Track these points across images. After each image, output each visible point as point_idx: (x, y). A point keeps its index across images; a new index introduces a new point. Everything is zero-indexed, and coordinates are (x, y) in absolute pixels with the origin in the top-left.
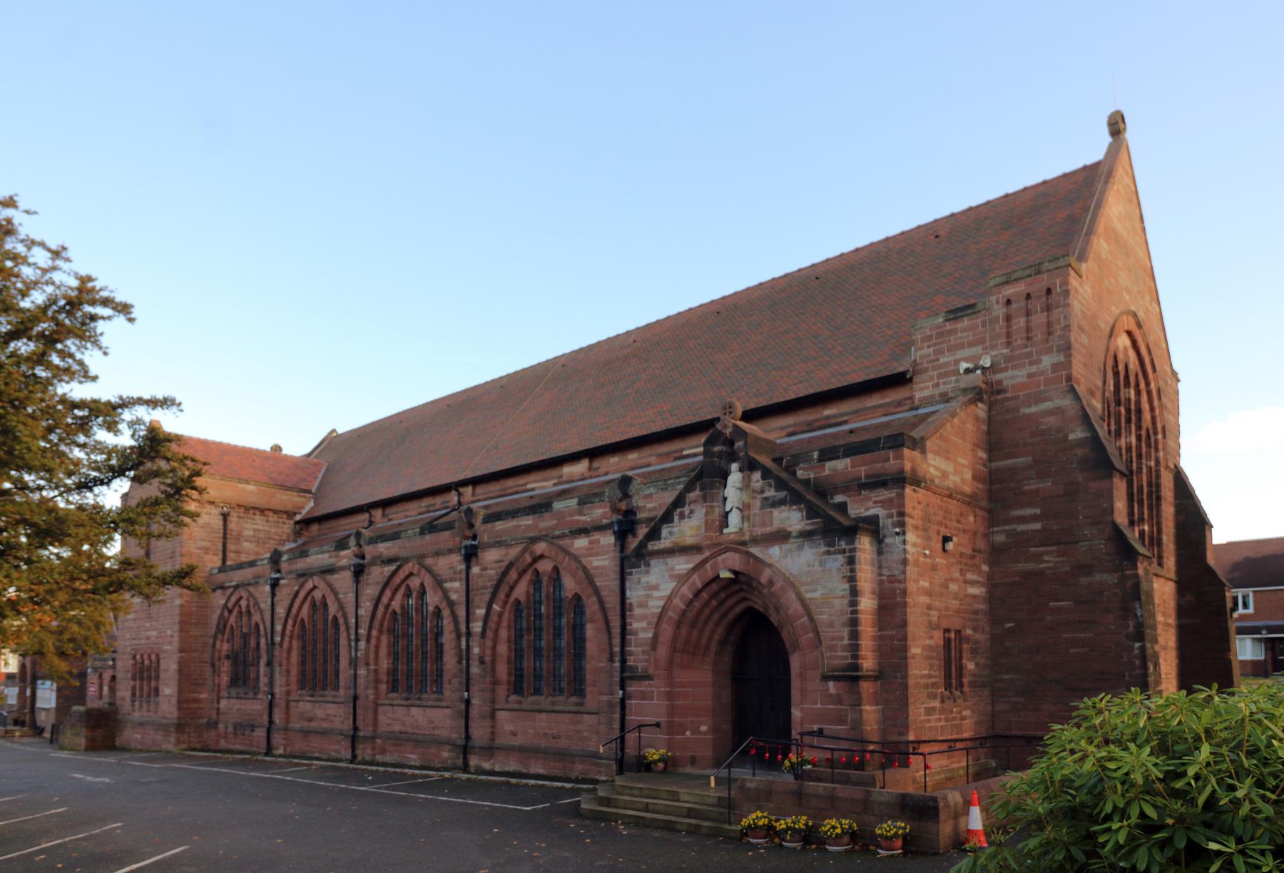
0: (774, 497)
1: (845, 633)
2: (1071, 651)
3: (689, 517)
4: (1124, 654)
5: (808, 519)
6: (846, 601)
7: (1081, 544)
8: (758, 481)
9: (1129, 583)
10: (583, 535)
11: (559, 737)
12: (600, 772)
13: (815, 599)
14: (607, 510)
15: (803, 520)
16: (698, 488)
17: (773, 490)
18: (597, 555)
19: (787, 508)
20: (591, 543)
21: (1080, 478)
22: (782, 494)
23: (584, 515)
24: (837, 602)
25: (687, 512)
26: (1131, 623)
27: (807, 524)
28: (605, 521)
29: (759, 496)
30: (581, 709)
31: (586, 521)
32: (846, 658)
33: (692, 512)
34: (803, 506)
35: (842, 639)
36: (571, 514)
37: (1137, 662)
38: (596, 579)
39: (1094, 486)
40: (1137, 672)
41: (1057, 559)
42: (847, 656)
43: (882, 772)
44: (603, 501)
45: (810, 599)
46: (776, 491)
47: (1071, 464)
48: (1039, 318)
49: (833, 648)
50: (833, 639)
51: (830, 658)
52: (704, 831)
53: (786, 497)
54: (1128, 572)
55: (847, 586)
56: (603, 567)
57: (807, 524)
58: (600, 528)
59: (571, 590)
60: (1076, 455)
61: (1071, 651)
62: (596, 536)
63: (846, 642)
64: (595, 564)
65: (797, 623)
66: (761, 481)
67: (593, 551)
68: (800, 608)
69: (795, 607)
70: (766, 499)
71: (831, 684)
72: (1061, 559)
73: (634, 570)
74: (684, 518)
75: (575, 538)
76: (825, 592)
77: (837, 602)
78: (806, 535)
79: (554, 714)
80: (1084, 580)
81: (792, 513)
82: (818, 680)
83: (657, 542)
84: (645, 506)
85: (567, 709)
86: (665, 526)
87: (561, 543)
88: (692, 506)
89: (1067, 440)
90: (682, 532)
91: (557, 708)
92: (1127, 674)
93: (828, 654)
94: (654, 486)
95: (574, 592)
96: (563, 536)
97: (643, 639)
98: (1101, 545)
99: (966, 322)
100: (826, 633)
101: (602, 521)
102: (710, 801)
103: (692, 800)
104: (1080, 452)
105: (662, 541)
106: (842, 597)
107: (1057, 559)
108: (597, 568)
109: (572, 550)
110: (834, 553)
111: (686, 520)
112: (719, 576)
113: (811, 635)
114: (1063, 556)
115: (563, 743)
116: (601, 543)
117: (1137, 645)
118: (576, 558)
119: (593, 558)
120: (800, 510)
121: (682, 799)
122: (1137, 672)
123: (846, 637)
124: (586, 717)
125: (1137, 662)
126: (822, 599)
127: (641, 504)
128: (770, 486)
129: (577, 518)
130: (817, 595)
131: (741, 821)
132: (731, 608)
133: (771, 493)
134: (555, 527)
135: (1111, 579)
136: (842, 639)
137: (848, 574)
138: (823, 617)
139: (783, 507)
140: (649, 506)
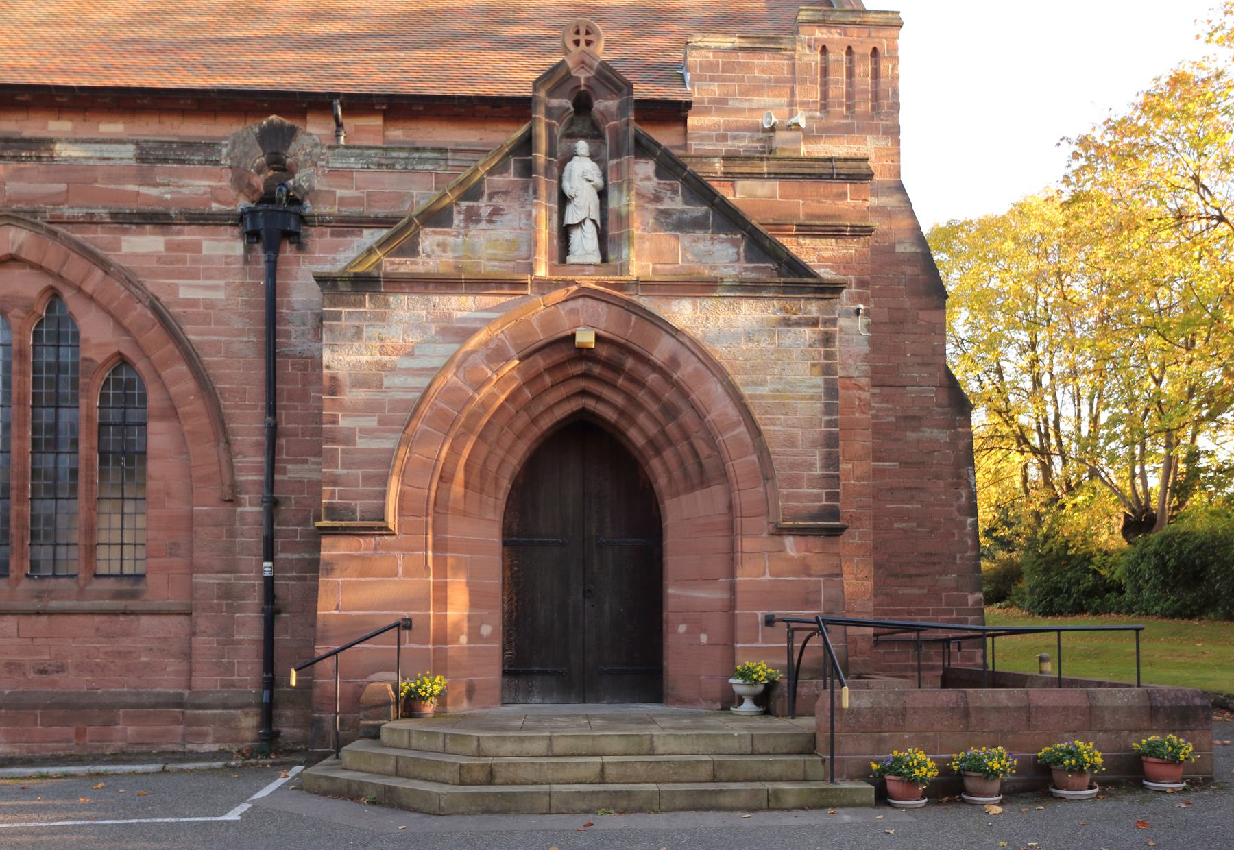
0: (683, 212)
1: (817, 457)
2: (896, 526)
3: (491, 222)
4: (955, 531)
5: (749, 260)
6: (819, 406)
7: (908, 388)
8: (648, 179)
9: (962, 444)
10: (148, 227)
11: (61, 669)
12: (202, 736)
13: (762, 397)
14: (225, 184)
15: (738, 260)
16: (512, 171)
17: (679, 199)
18: (193, 275)
19: (708, 236)
20: (169, 247)
21: (907, 303)
22: (700, 210)
23: (157, 185)
24: (801, 405)
25: (485, 211)
26: (964, 493)
27: (746, 269)
28: (215, 207)
29: (650, 206)
30: (132, 605)
31: (160, 200)
32: (817, 498)
33: (496, 211)
34: (739, 236)
35: (811, 466)
36: (120, 177)
37: (970, 542)
38: (188, 328)
39: (925, 316)
40: (969, 554)
41: (880, 406)
42: (820, 495)
43: (996, 670)
44: (217, 163)
45: (752, 396)
46: (686, 203)
47: (899, 284)
48: (449, 155)
49: (793, 482)
50: (793, 466)
51: (789, 497)
52: (790, 801)
53: (706, 216)
54: (960, 430)
55: (819, 380)
56: (209, 304)
57: (746, 269)
58: (201, 219)
59: (100, 345)
60: (903, 273)
61: (896, 526)
62: (189, 235)
63: (818, 472)
64: (184, 293)
65: (727, 436)
66: (656, 179)
67: (174, 267)
68: (733, 413)
69: (720, 408)
70: (665, 213)
71: (789, 541)
72: (885, 405)
73: (344, 310)
74: (478, 221)
75: (126, 232)
76: (780, 387)
77: (801, 405)
78: (749, 288)
79: (44, 619)
80: (912, 436)
81: (718, 246)
82: (765, 535)
83: (409, 260)
84: (333, 193)
85: (87, 605)
86: (428, 230)
87: (78, 236)
88: (499, 202)
89: (894, 252)
90: (472, 249)
91: (54, 605)
92: (958, 556)
93: (785, 492)
94: (356, 156)
95: (115, 350)
96: (90, 221)
97: (363, 451)
98: (932, 393)
99: (766, 59)
100: (781, 456)
101: (207, 203)
102: (734, 745)
103: (688, 749)
104: (909, 270)
105: (419, 259)
106: (812, 398)
107: (880, 406)
108: (193, 303)
109: (113, 257)
110: (798, 324)
111: (483, 225)
112: (573, 336)
113: (754, 458)
114: (887, 402)
115: (73, 682)
116: (204, 252)
117: (970, 520)
118: (128, 279)
119: (182, 281)
120: (735, 244)
121: (660, 750)
122: (969, 554)
123: (818, 465)
124: (144, 620)
125: (970, 542)
126: (774, 397)
127: (319, 184)
128: (675, 192)
129: (132, 187)
130: (764, 390)
131: (1099, 751)
132: (550, 409)
133: (676, 203)
134: (64, 198)
135: (943, 436)
136: (811, 466)
137: (822, 361)
138: (772, 429)
139: (699, 233)
140: (339, 193)
